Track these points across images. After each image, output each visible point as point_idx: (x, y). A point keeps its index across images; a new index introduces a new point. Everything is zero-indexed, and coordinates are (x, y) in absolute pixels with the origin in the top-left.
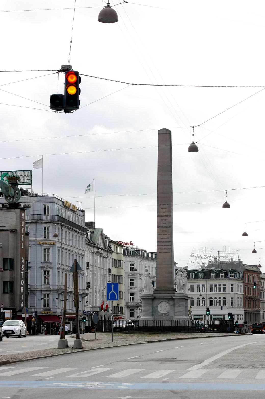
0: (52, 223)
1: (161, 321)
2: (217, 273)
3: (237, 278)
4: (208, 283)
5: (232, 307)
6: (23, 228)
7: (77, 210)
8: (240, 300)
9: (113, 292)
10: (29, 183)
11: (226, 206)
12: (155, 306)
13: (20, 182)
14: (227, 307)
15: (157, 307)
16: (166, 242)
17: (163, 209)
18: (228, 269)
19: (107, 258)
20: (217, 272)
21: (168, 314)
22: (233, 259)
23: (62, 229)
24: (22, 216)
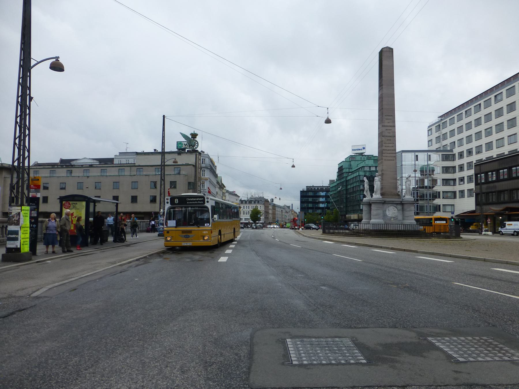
1: (394, 225)
16: (391, 150)
21: (396, 218)
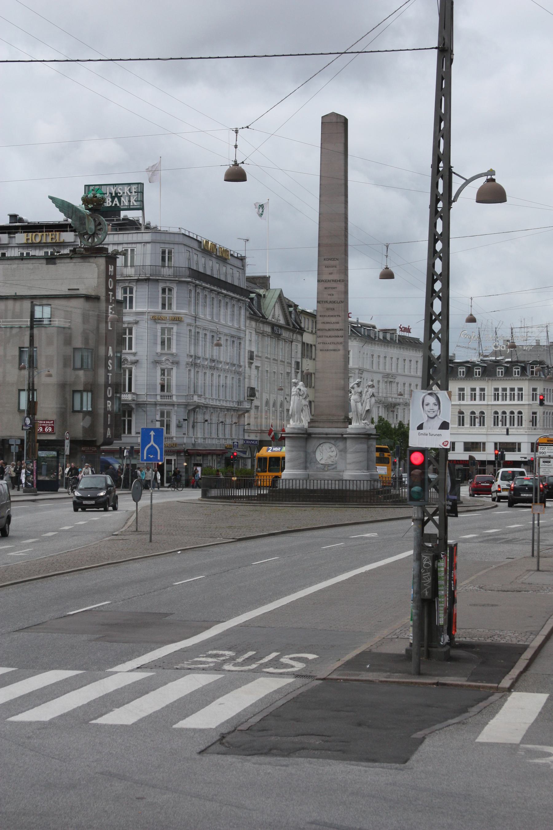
0: (178, 282)
1: (323, 482)
2: (507, 367)
3: (543, 377)
4: (489, 386)
5: (535, 429)
6: (111, 293)
7: (228, 255)
8: (550, 417)
9: (152, 445)
10: (137, 207)
11: (387, 275)
12: (310, 450)
13: (122, 205)
14: (524, 428)
15: (315, 452)
16: (333, 330)
17: (328, 267)
18: (529, 360)
19: (292, 342)
20: (508, 365)
22: (539, 343)
23: (197, 291)
24: (110, 269)
